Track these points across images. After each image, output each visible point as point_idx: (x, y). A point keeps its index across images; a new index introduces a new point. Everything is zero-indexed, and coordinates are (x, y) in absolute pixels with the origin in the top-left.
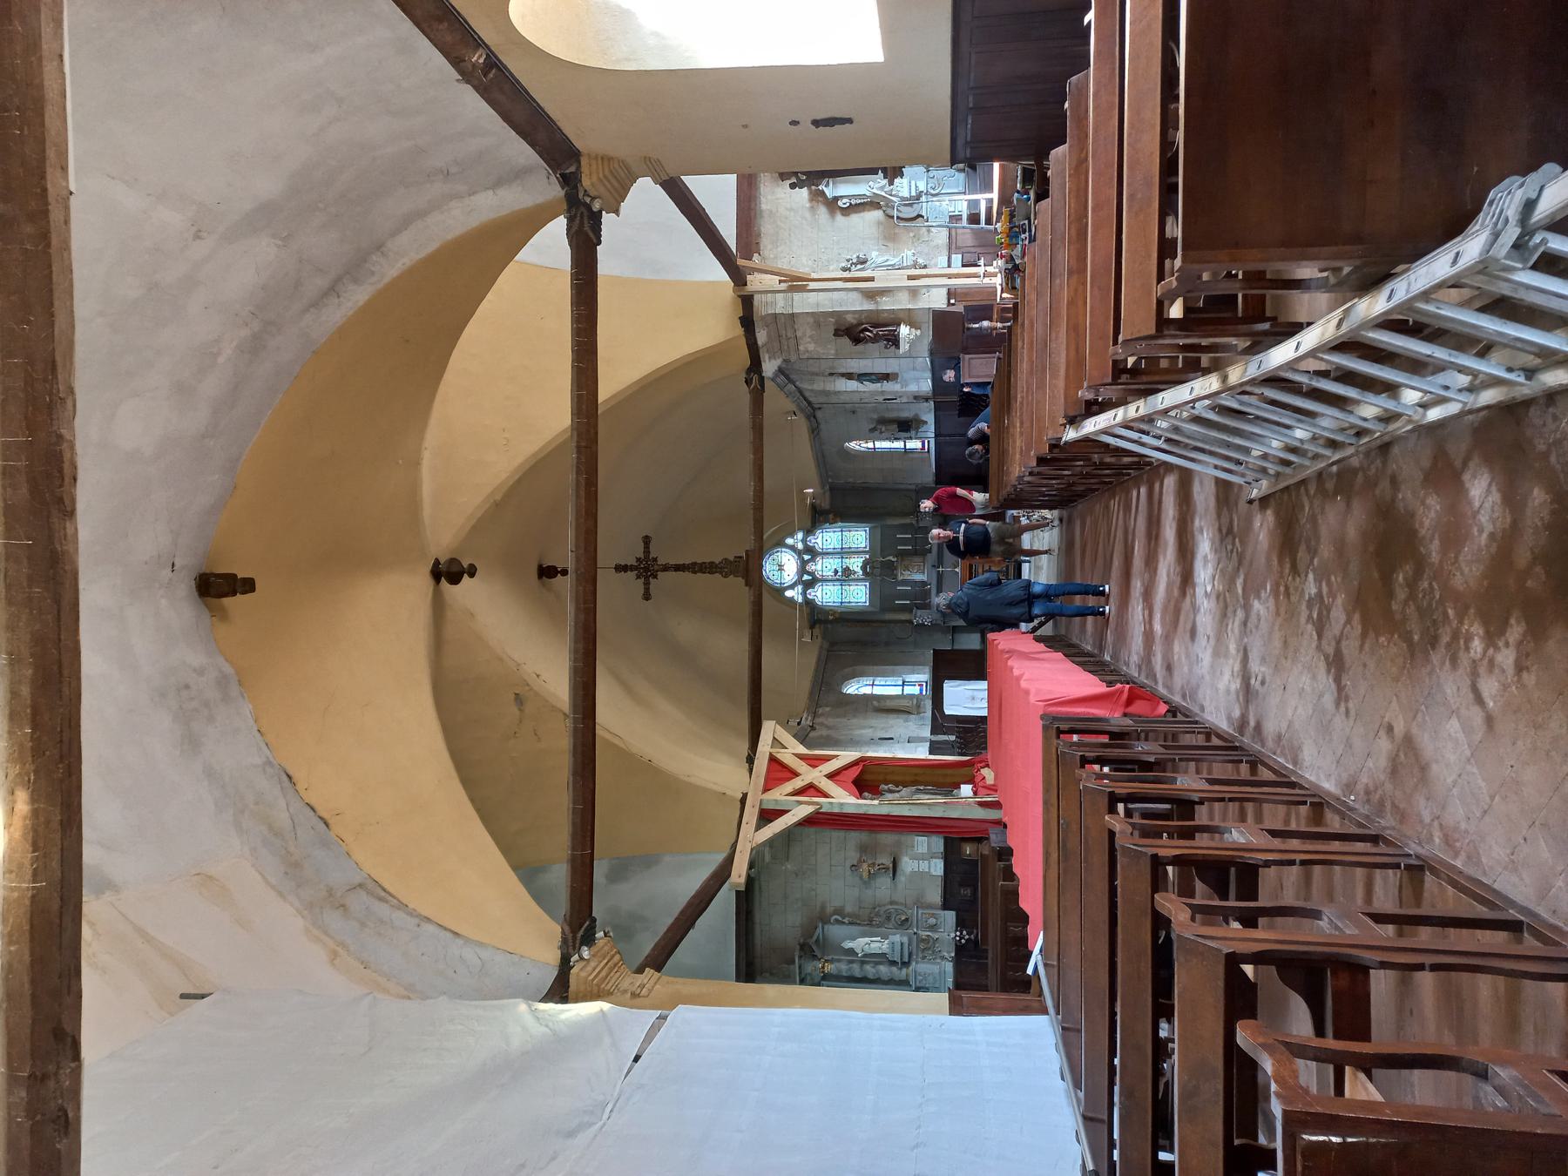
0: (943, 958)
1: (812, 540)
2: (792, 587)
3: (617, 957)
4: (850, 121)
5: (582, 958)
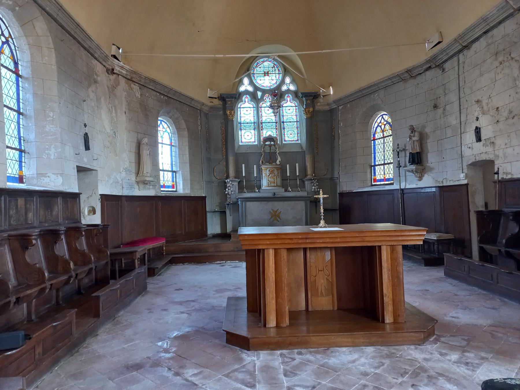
2: (251, 83)
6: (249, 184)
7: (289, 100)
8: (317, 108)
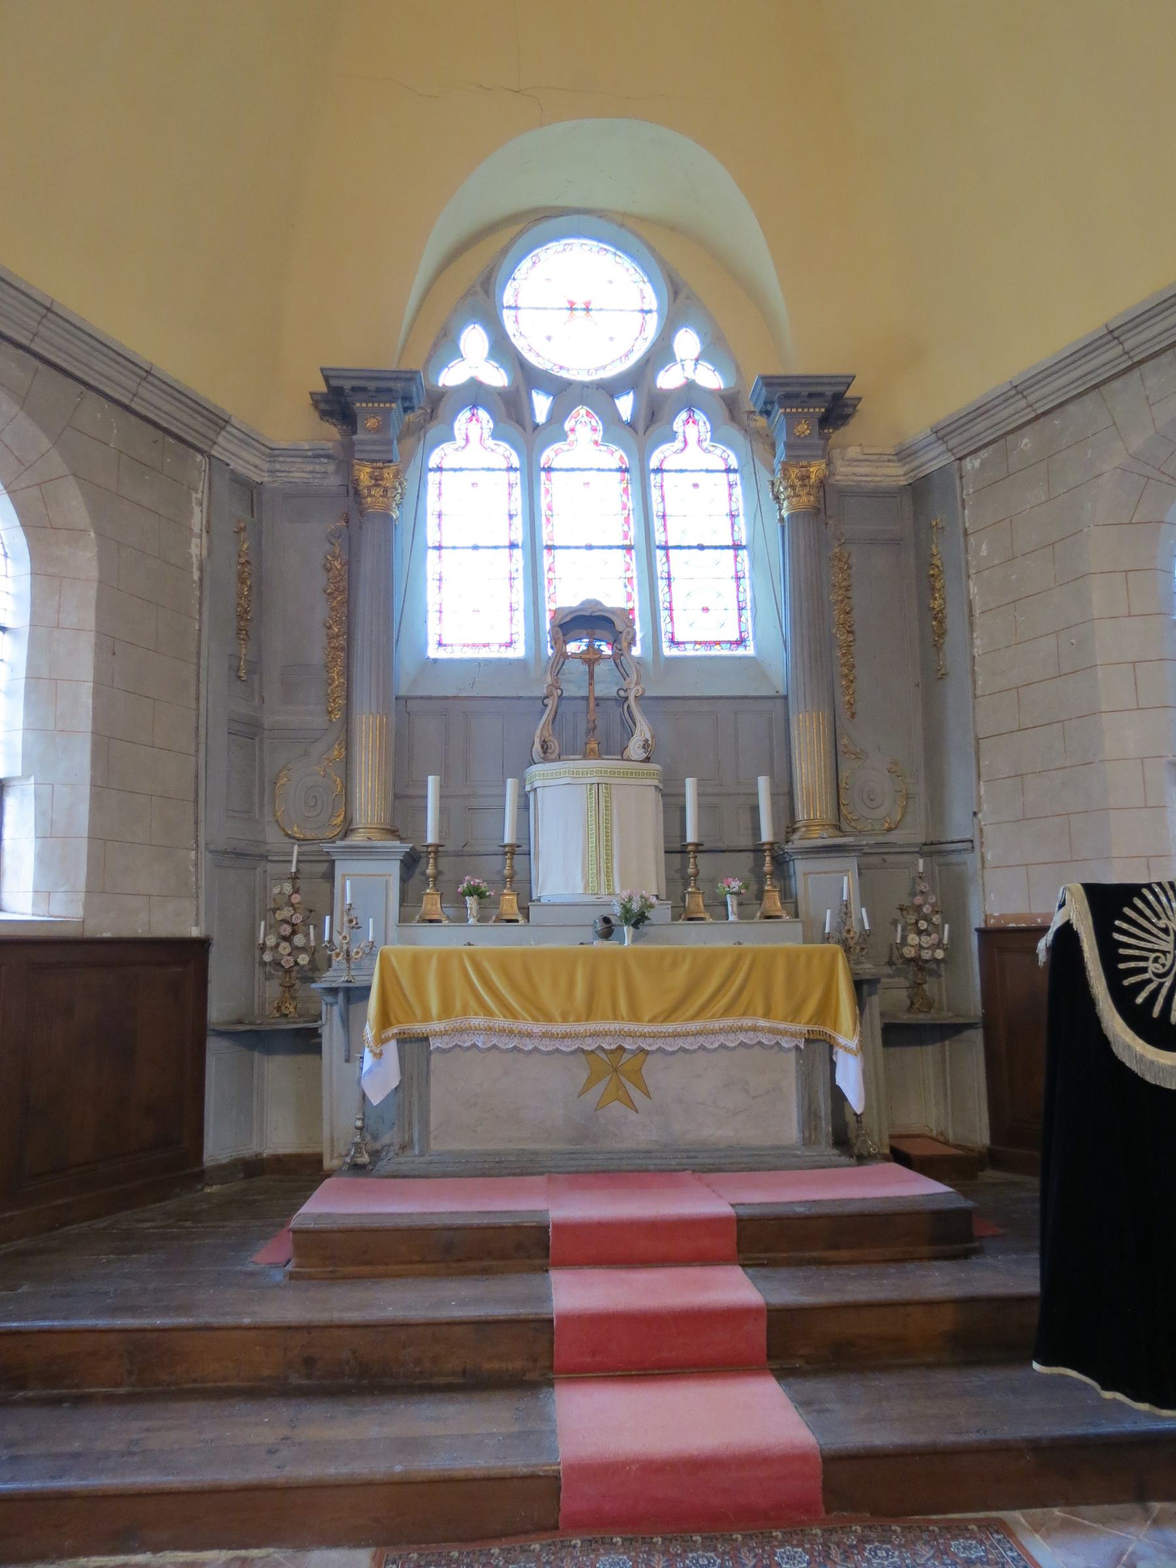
1: (692, 429)
2: (502, 349)
7: (692, 440)
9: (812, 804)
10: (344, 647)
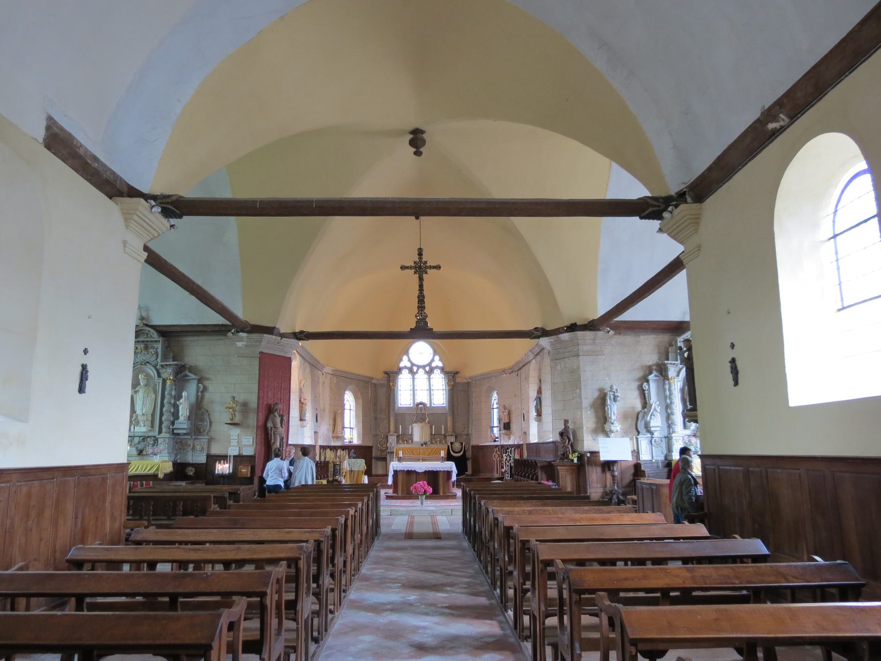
0: (176, 455)
2: (409, 360)
3: (156, 234)
4: (736, 383)
5: (153, 207)
6: (404, 437)
8: (457, 381)
9: (450, 429)
10: (389, 406)
